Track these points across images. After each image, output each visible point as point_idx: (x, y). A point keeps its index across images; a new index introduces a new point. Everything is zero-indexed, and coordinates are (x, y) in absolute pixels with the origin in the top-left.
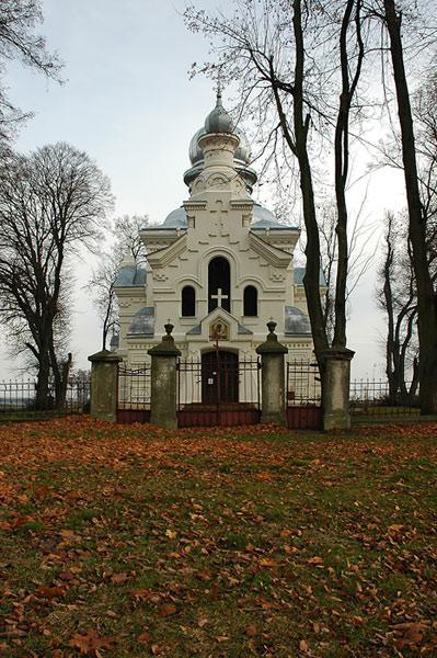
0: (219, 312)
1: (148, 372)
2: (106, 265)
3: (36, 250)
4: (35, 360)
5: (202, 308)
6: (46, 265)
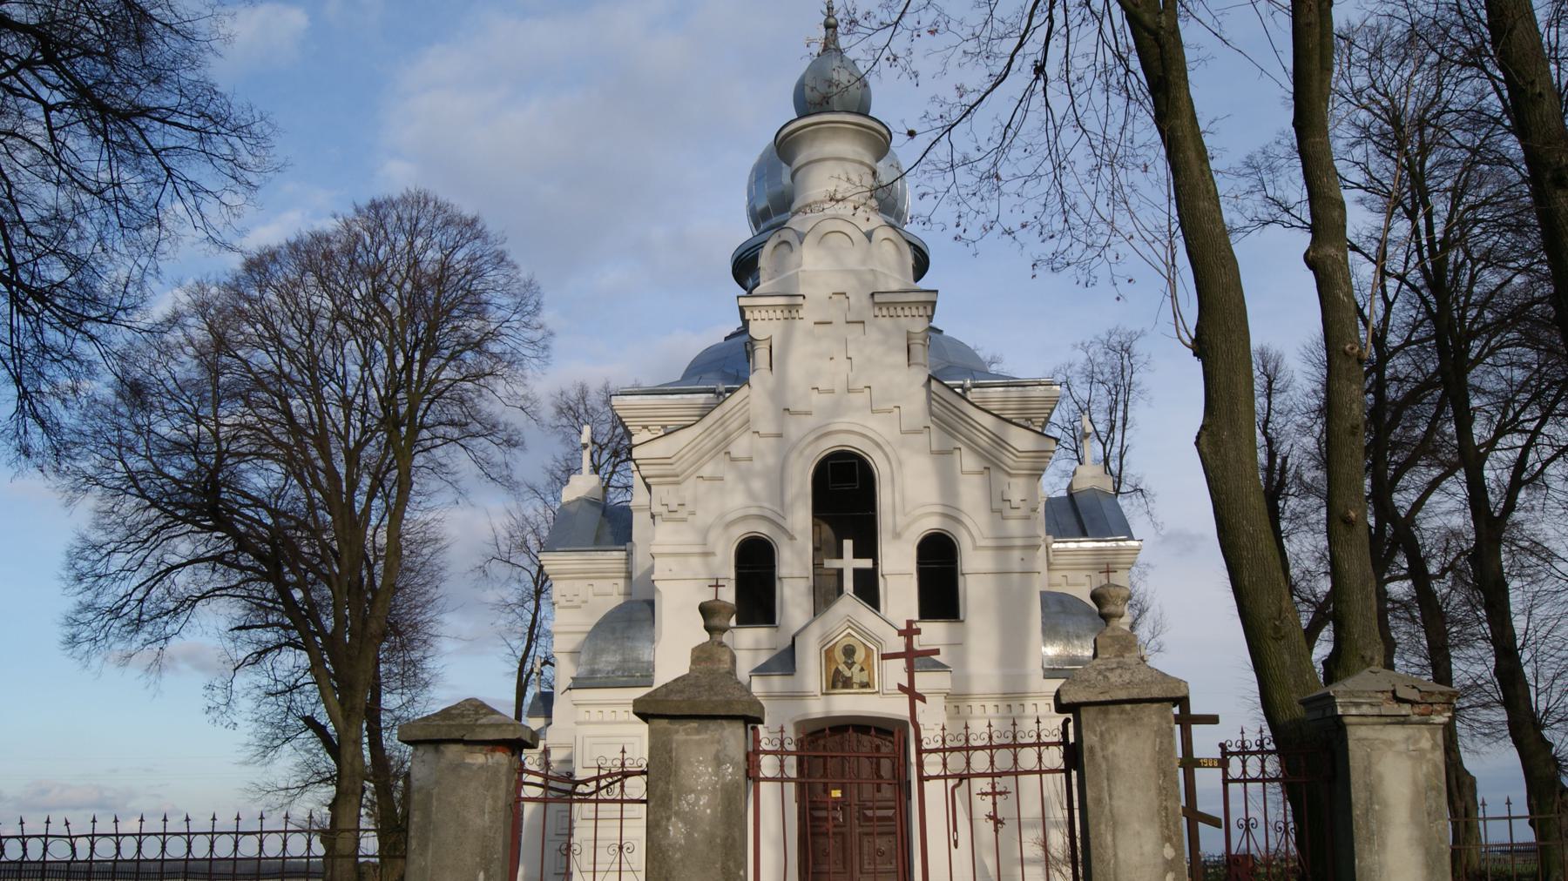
0: (849, 605)
1: (636, 787)
2: (529, 512)
3: (342, 470)
4: (327, 763)
5: (793, 592)
6: (367, 510)
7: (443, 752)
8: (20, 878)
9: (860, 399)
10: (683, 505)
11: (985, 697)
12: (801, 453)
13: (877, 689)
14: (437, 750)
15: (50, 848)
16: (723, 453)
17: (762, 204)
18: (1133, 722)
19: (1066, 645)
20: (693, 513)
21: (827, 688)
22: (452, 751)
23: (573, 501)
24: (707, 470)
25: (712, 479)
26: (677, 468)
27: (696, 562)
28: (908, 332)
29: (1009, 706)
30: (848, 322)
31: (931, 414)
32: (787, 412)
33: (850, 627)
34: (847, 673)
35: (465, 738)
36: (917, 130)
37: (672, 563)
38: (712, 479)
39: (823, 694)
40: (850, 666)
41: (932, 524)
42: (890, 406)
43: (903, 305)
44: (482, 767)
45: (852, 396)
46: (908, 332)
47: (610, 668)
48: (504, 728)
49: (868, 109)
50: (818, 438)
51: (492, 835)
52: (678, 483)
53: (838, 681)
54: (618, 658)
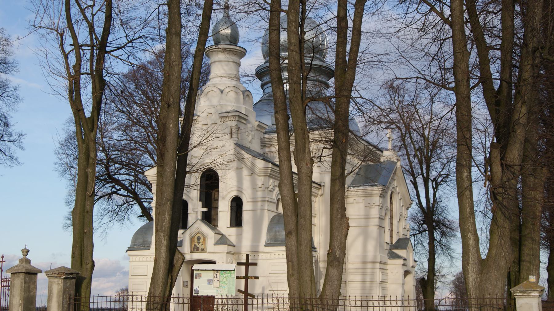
8: (385, 306)
18: (18, 277)
34: (198, 246)
40: (199, 243)
41: (234, 194)
53: (195, 249)
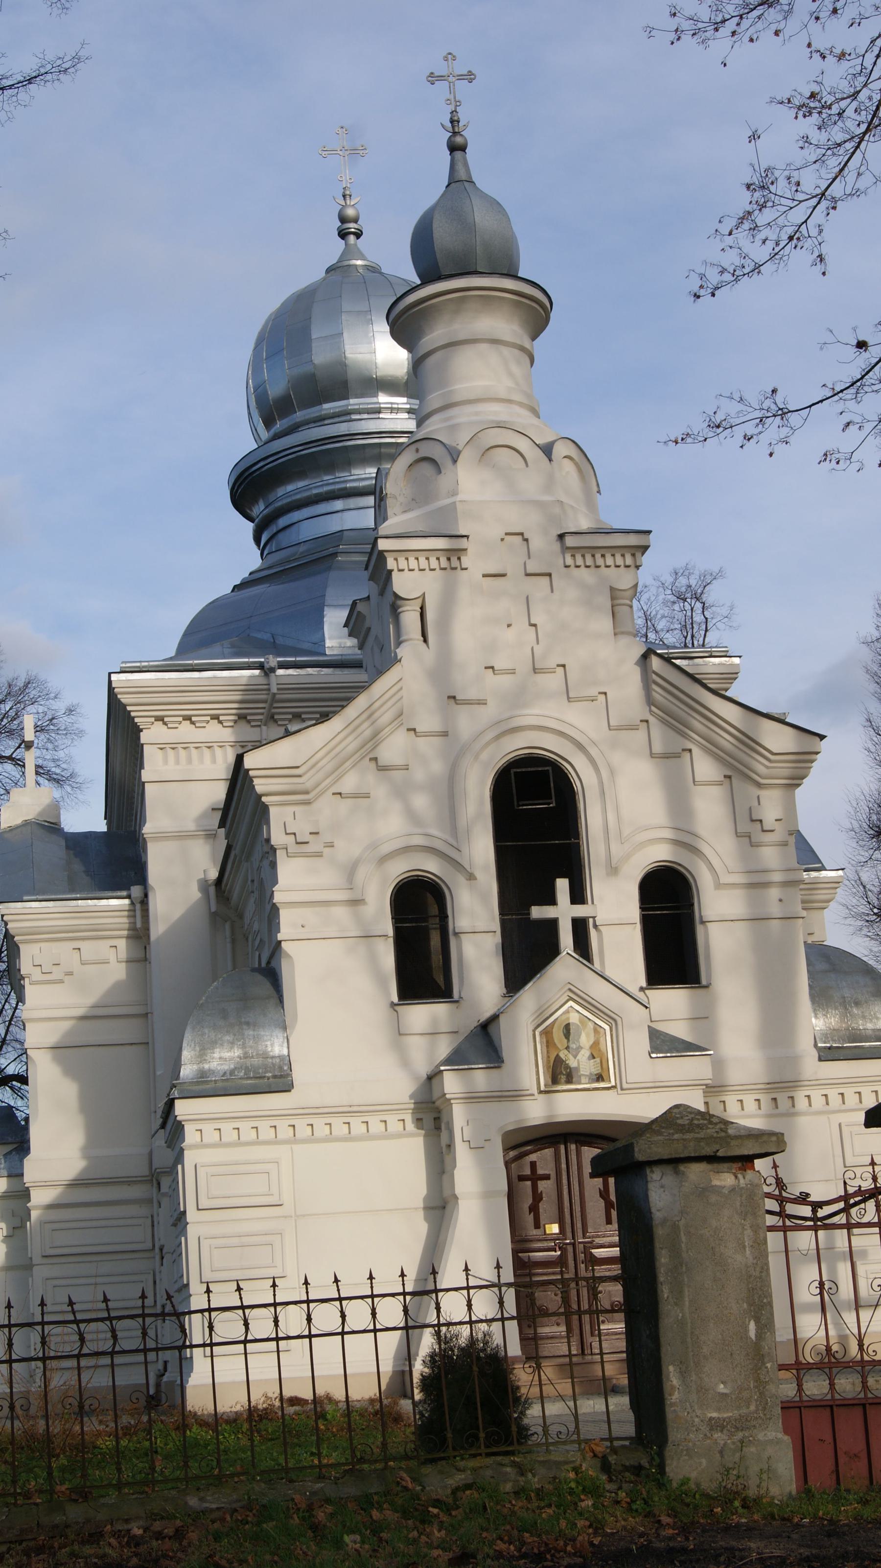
7: (683, 1173)
9: (554, 681)
10: (317, 833)
11: (745, 1088)
12: (477, 757)
13: (613, 1083)
14: (677, 1172)
15: (216, 1325)
16: (367, 759)
17: (275, 390)
19: (846, 1012)
20: (331, 845)
21: (546, 1085)
22: (695, 1171)
23: (17, 827)
24: (350, 783)
25: (356, 796)
26: (307, 782)
27: (341, 913)
28: (612, 589)
29: (775, 1099)
30: (527, 575)
31: (650, 701)
32: (452, 701)
33: (571, 999)
35: (720, 1154)
36: (870, 342)
37: (308, 915)
38: (356, 796)
39: (541, 1092)
42: (593, 691)
43: (603, 551)
44: (733, 1190)
45: (539, 677)
46: (612, 589)
47: (226, 1067)
48: (765, 1138)
49: (517, 271)
50: (498, 737)
51: (757, 1274)
52: (308, 803)
54: (237, 1052)
